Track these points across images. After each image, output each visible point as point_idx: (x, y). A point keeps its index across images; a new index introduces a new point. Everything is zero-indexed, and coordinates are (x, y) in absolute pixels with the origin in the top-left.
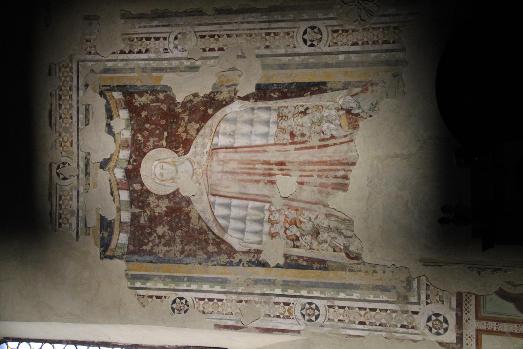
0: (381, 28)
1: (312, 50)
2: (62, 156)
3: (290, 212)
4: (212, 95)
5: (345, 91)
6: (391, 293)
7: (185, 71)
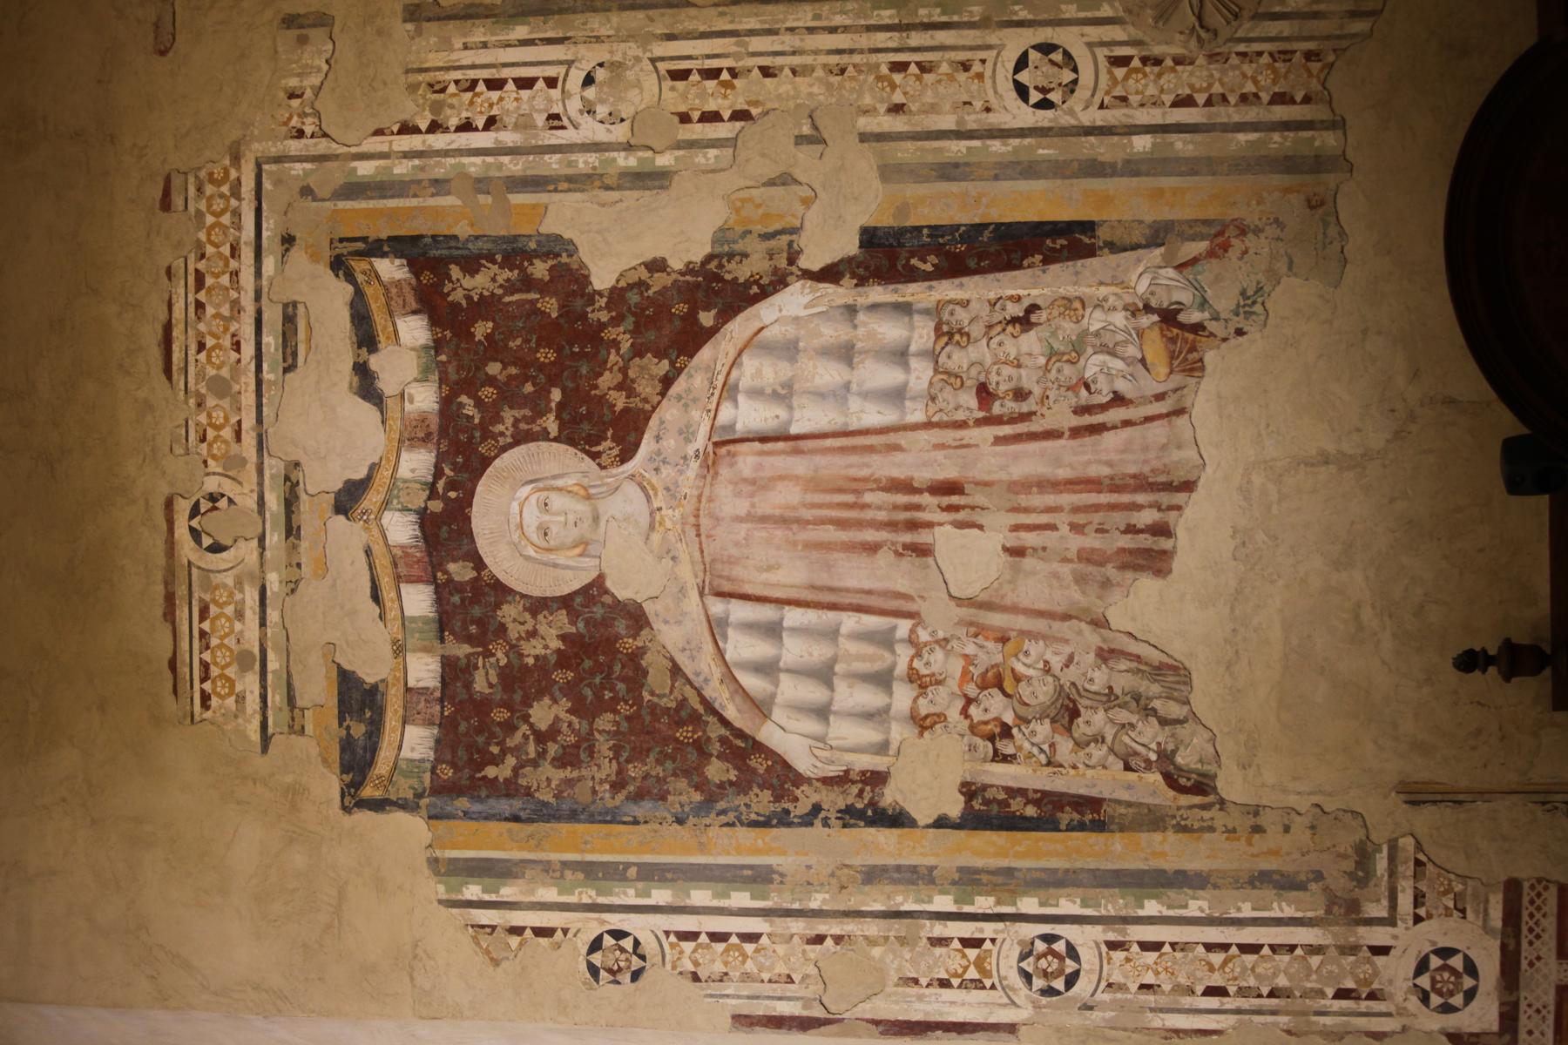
0: (1266, 55)
1: (1044, 118)
2: (208, 474)
3: (982, 647)
4: (712, 266)
5: (1158, 251)
6: (1309, 893)
7: (619, 188)
